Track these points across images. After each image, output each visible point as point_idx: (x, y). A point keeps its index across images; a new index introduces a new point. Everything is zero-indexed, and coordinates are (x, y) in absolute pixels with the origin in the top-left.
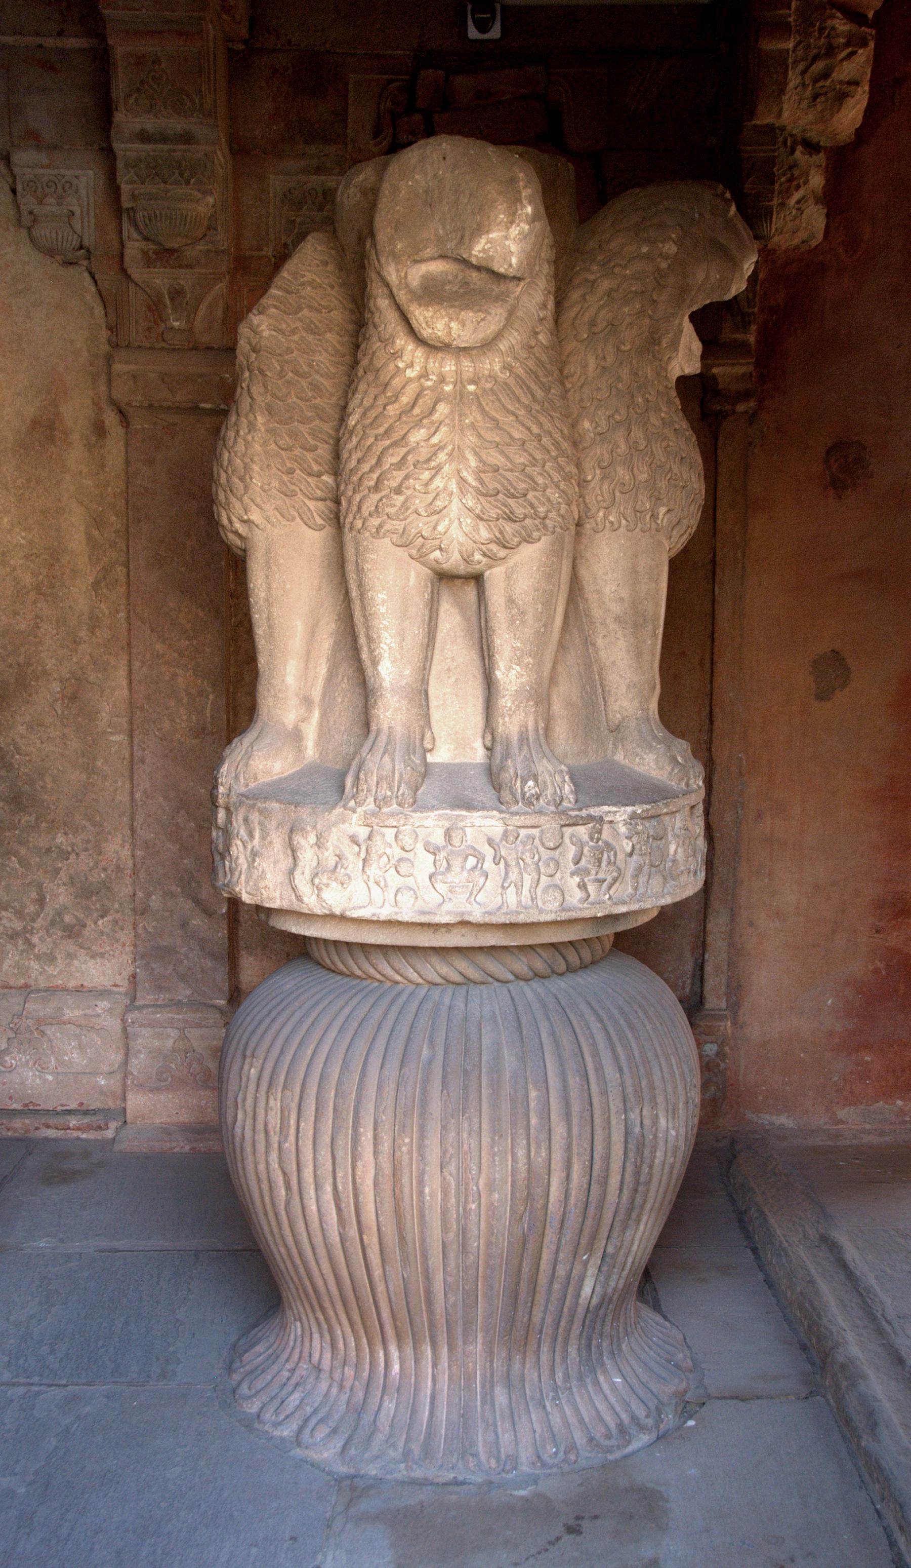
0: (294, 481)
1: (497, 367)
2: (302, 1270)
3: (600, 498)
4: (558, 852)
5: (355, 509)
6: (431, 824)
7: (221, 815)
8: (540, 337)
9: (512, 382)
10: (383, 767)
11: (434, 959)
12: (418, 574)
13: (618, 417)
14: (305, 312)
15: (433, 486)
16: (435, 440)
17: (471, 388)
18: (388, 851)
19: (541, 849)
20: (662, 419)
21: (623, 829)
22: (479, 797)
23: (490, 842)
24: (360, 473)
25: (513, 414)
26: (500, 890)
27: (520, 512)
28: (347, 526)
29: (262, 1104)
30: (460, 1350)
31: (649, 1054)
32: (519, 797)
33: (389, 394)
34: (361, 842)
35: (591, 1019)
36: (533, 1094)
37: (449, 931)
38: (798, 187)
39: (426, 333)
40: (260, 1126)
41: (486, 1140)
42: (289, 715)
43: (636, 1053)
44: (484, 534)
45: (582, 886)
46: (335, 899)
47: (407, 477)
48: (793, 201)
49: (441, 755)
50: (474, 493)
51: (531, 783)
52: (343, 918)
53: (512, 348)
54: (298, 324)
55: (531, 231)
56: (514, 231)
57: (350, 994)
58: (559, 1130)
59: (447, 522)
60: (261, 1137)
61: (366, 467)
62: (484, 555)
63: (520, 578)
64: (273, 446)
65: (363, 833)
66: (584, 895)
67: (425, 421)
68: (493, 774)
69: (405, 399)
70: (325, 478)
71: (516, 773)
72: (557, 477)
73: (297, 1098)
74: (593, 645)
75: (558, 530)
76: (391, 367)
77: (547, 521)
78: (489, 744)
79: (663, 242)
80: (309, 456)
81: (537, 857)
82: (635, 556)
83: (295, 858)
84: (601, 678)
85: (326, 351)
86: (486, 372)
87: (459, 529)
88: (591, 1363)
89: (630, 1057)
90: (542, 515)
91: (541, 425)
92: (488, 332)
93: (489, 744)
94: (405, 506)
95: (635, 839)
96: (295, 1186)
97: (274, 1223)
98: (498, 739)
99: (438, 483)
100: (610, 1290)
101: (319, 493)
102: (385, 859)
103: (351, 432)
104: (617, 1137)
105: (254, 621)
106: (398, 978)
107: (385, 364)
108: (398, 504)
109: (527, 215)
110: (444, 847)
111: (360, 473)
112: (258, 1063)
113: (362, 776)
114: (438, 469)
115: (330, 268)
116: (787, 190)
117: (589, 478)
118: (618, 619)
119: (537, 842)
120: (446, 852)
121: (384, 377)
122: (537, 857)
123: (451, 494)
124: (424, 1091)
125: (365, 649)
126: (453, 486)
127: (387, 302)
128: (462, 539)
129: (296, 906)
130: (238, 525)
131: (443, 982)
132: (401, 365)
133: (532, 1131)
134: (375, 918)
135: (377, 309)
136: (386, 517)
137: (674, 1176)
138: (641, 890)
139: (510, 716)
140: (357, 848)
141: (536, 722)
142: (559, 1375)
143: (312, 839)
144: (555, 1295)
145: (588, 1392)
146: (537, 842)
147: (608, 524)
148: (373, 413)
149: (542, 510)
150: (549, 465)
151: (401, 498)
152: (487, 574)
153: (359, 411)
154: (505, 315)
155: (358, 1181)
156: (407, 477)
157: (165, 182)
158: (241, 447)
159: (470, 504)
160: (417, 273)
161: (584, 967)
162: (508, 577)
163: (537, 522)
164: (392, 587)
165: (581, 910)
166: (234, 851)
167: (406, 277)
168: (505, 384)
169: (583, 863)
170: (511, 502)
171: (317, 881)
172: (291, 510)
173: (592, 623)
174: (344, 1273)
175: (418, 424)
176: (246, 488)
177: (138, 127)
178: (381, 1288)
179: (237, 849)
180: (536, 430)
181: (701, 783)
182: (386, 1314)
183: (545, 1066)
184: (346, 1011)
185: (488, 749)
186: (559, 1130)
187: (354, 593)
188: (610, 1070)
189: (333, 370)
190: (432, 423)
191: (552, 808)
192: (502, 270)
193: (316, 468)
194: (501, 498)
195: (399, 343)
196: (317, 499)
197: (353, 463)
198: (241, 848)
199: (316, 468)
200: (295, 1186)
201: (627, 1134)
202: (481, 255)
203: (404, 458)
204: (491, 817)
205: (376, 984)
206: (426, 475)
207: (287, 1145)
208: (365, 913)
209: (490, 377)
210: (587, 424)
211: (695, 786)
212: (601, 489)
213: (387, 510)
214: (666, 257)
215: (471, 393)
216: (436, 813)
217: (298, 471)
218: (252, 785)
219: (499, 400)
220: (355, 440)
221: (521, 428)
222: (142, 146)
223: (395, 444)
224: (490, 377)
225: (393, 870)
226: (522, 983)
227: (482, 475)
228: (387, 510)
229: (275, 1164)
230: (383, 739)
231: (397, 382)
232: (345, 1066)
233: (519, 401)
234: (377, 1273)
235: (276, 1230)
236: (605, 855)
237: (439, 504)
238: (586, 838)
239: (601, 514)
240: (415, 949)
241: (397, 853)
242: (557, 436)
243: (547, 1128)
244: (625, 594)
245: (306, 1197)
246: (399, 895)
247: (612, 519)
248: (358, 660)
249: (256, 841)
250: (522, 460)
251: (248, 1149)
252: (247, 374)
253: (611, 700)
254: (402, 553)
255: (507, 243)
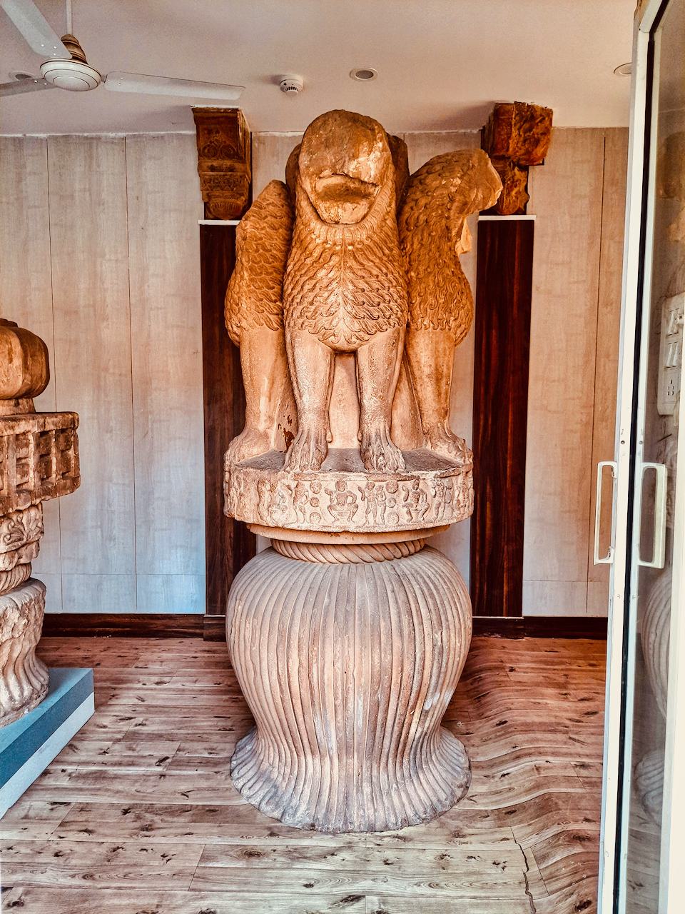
0: (263, 305)
1: (364, 237)
2: (263, 714)
3: (419, 312)
4: (396, 494)
5: (290, 315)
6: (329, 480)
7: (227, 475)
8: (387, 222)
9: (372, 245)
10: (304, 452)
11: (333, 550)
12: (323, 350)
13: (429, 270)
14: (269, 218)
15: (329, 301)
16: (330, 275)
17: (350, 248)
18: (306, 493)
19: (386, 492)
20: (453, 272)
21: (430, 484)
22: (355, 466)
23: (360, 489)
24: (293, 295)
25: (372, 261)
26: (365, 514)
27: (376, 314)
28: (287, 325)
29: (243, 626)
30: (345, 761)
31: (445, 602)
32: (375, 466)
33: (308, 253)
34: (292, 488)
35: (414, 583)
36: (383, 624)
37: (338, 535)
38: (516, 186)
39: (325, 216)
40: (242, 637)
41: (357, 650)
42: (262, 426)
43: (438, 602)
44: (357, 326)
45: (409, 513)
46: (279, 518)
47: (316, 296)
48: (513, 193)
49: (337, 445)
50: (351, 304)
51: (381, 458)
52: (283, 529)
53: (372, 227)
54: (265, 225)
55: (382, 156)
56: (372, 156)
57: (291, 567)
58: (397, 643)
59: (337, 320)
60: (242, 643)
61: (295, 292)
62: (357, 338)
63: (377, 351)
64: (252, 287)
65: (293, 484)
66: (410, 518)
67: (326, 266)
68: (363, 454)
69: (315, 255)
70: (278, 303)
71: (373, 453)
72: (396, 297)
73: (260, 624)
74: (415, 389)
75: (397, 325)
76: (309, 238)
77: (391, 320)
78: (360, 439)
79: (453, 178)
80: (270, 292)
81: (384, 497)
82: (437, 343)
83: (260, 497)
84: (419, 407)
85: (279, 238)
86: (358, 240)
87: (344, 329)
88: (417, 768)
89: (435, 604)
90: (388, 317)
91: (387, 268)
92: (359, 215)
93: (360, 439)
94: (315, 312)
95: (437, 489)
96: (259, 671)
97: (248, 689)
98: (365, 436)
99: (332, 298)
100: (425, 729)
101: (275, 311)
102: (305, 497)
103: (289, 275)
104: (429, 648)
105: (244, 378)
106: (314, 559)
107: (306, 237)
108: (312, 310)
109: (379, 147)
110: (335, 492)
111: (293, 295)
112: (242, 603)
113: (293, 454)
114: (333, 290)
115: (282, 196)
116: (511, 187)
117: (414, 302)
118: (428, 376)
119: (385, 489)
120: (340, 497)
121: (305, 244)
122: (384, 497)
123: (339, 305)
124: (325, 621)
125: (296, 389)
126: (340, 299)
127: (306, 203)
128: (346, 329)
129: (261, 522)
130: (235, 329)
131: (349, 562)
132: (314, 237)
133: (382, 645)
134: (300, 529)
135: (301, 207)
136: (305, 318)
137: (459, 668)
138: (440, 515)
139: (371, 424)
140: (290, 492)
141: (385, 427)
142: (398, 775)
143: (268, 487)
144: (395, 736)
145: (414, 785)
146: (385, 489)
147: (423, 327)
148: (298, 265)
149: (388, 314)
150: (391, 289)
151: (313, 307)
152: (359, 350)
153: (292, 263)
154: (368, 206)
155: (290, 670)
156: (316, 296)
157: (222, 190)
158: (237, 289)
159: (350, 310)
160: (321, 185)
161: (410, 555)
162: (370, 351)
163: (385, 320)
164: (310, 357)
165: (408, 525)
166: (231, 493)
167: (315, 187)
168: (369, 246)
169: (409, 500)
170: (371, 308)
171: (270, 509)
172: (261, 320)
173: (415, 378)
174: (283, 717)
175: (322, 267)
176: (239, 309)
177: (210, 164)
178: (302, 727)
179: (233, 493)
180: (385, 271)
181: (471, 461)
182: (306, 741)
183: (389, 609)
184: (287, 577)
185: (360, 441)
186: (397, 643)
187: (290, 360)
188: (424, 611)
189: (283, 249)
190: (329, 266)
191: (393, 472)
192: (366, 180)
193: (274, 298)
194: (365, 309)
195: (312, 225)
196: (274, 314)
197: (289, 291)
198: (235, 492)
199: (274, 298)
200: (259, 671)
201: (434, 646)
202: (355, 171)
203: (315, 286)
204: (360, 476)
205: (304, 562)
206: (326, 294)
207: (254, 648)
208: (294, 526)
209: (361, 242)
210: (413, 274)
211: (468, 463)
212: (420, 307)
213: (306, 314)
214: (455, 186)
215: (349, 251)
216: (332, 473)
217: (264, 300)
218: (242, 461)
219: (364, 253)
220: (290, 278)
221: (377, 269)
222: (211, 173)
223: (311, 278)
224: (361, 242)
225: (309, 503)
226: (378, 563)
227: (356, 294)
228: (306, 314)
229: (248, 658)
230: (305, 436)
231: (311, 247)
232: (285, 607)
233: (375, 255)
234: (301, 719)
235: (250, 692)
236: (421, 496)
237: (333, 310)
238: (410, 488)
239: (420, 320)
240: (322, 545)
241: (311, 495)
242: (397, 275)
243: (390, 643)
244: (432, 363)
245: (263, 677)
246: (312, 517)
247: (425, 323)
248: (293, 395)
249: (242, 488)
250: (377, 286)
251: (236, 649)
252: (240, 252)
253: (425, 417)
254: (315, 338)
255: (368, 163)
